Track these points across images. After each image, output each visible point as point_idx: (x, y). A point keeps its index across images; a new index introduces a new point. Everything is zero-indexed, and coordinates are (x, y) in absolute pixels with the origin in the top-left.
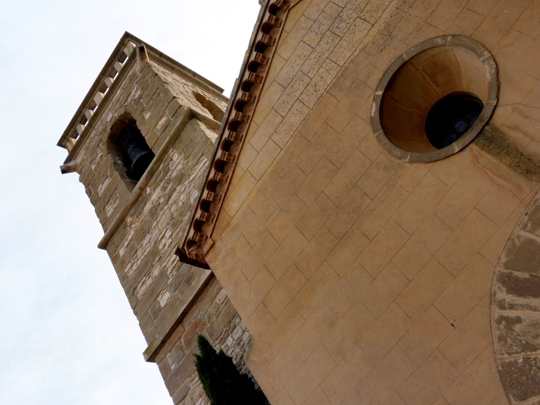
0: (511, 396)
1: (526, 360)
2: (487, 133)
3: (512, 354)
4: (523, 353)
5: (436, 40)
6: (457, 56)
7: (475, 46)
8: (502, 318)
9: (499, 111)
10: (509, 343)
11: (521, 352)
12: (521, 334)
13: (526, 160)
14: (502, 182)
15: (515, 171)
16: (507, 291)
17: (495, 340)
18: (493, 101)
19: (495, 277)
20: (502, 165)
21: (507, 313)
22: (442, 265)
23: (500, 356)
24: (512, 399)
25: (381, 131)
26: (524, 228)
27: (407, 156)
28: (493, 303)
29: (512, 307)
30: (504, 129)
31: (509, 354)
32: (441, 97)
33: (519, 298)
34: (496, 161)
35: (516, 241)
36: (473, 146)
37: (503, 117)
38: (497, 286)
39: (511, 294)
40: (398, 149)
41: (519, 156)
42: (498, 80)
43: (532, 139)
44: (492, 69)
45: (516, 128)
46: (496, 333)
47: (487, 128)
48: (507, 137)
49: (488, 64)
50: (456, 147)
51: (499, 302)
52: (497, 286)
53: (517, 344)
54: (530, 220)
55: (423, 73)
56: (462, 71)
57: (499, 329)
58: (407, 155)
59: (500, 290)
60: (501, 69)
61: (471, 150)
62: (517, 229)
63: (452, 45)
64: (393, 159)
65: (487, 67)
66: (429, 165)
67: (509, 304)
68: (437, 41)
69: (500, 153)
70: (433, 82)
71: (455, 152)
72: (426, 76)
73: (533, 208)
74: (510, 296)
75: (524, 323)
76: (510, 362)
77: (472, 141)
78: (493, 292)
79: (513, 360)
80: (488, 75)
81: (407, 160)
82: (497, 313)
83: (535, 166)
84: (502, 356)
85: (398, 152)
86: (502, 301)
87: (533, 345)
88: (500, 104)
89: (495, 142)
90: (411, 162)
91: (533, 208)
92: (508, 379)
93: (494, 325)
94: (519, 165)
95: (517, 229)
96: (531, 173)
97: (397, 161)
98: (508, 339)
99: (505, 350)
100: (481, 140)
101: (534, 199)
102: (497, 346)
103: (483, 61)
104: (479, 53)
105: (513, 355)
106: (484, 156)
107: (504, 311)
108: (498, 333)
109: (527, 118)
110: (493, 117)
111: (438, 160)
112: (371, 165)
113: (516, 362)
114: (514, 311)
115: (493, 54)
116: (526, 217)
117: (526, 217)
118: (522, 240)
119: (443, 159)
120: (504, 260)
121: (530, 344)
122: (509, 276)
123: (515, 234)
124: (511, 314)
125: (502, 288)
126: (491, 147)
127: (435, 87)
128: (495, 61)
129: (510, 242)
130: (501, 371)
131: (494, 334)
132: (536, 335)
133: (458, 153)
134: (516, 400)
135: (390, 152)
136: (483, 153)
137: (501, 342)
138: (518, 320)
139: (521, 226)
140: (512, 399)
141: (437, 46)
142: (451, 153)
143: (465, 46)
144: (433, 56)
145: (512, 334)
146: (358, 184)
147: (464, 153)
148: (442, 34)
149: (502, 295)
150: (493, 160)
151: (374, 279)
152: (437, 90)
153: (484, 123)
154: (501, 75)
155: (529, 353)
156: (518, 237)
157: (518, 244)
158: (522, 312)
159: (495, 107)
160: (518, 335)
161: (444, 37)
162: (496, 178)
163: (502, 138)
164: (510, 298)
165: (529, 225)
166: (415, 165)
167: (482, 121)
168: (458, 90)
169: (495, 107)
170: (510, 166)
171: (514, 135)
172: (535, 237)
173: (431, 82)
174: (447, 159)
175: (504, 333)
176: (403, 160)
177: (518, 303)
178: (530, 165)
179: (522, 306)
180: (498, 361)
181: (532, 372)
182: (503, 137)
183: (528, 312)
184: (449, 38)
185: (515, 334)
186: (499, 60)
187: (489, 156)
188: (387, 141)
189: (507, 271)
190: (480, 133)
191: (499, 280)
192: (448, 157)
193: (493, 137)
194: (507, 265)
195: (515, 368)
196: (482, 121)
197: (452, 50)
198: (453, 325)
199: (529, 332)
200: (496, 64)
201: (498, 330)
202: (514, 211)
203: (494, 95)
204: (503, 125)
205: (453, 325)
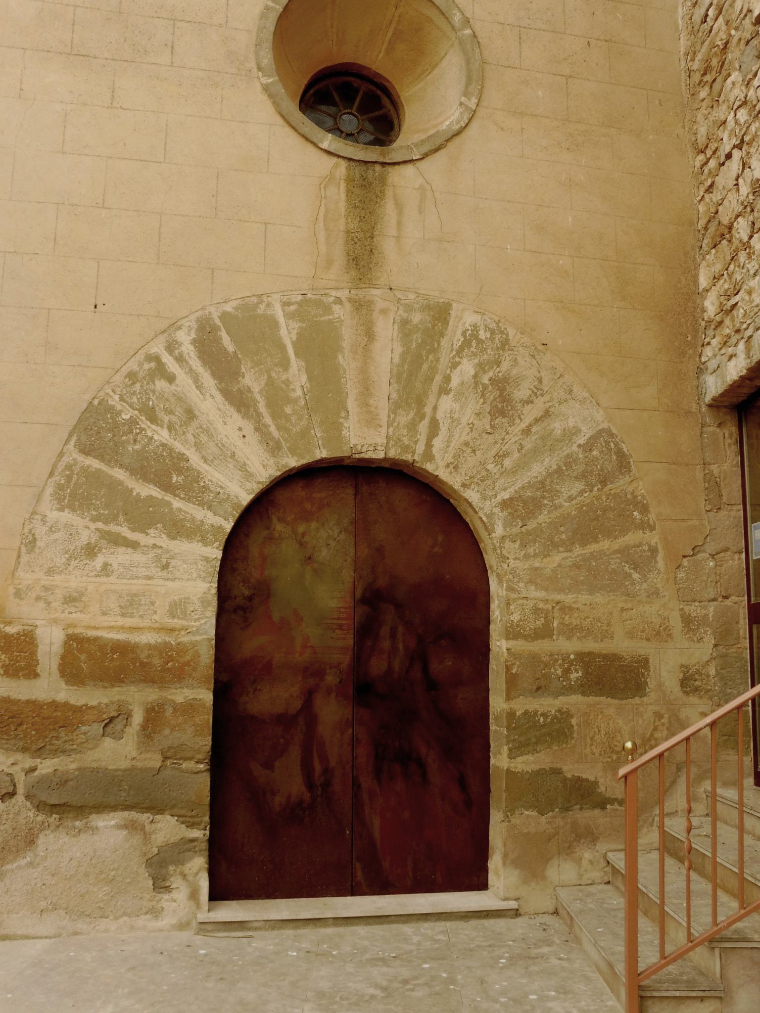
0: (74, 438)
1: (133, 421)
2: (370, 172)
3: (125, 401)
4: (136, 412)
5: (456, 11)
6: (448, 57)
7: (475, 79)
8: (157, 359)
9: (409, 169)
10: (134, 389)
11: (137, 409)
12: (157, 393)
13: (368, 248)
14: (322, 236)
15: (347, 243)
16: (194, 339)
17: (125, 370)
18: (416, 153)
19: (199, 314)
20: (342, 221)
21: (167, 359)
22: (160, 233)
23: (109, 391)
24: (72, 442)
25: (280, 9)
26: (286, 304)
27: (269, 76)
28: (166, 334)
29: (180, 359)
30: (389, 193)
31: (122, 399)
32: (374, 68)
33: (197, 360)
34: (343, 210)
35: (262, 306)
36: (343, 164)
37: (404, 180)
38: (189, 323)
39: (195, 347)
40: (270, 56)
41: (368, 235)
42: (447, 141)
43: (398, 238)
44: (458, 123)
45: (399, 207)
46: (133, 365)
47: (378, 168)
48: (382, 203)
49: (461, 113)
50: (328, 141)
51: (174, 341)
52: (189, 323)
53: (141, 398)
54: (300, 304)
55: (396, 18)
56: (429, 78)
57: (141, 364)
58: (272, 76)
59: (189, 331)
60: (463, 135)
61: (336, 166)
62: (276, 296)
63: (461, 42)
64: (252, 57)
65: (457, 114)
66: (280, 121)
67: (181, 355)
68: (455, 15)
69: (356, 207)
70: (390, 42)
71: (320, 145)
72: (394, 25)
73: (316, 297)
74: (192, 348)
75: (173, 387)
76: (113, 406)
77: (350, 159)
78: (179, 324)
79: (119, 408)
80: (447, 123)
81: (265, 80)
82: (158, 347)
83: (368, 264)
84: (112, 394)
85: (267, 59)
86: (177, 343)
87: (156, 416)
88: (418, 164)
89: (366, 193)
90: (266, 88)
91: (316, 297)
92: (92, 420)
93: (141, 355)
94: (356, 243)
95: (276, 296)
96: (356, 265)
97: (252, 65)
98: (138, 385)
99: (122, 391)
100: (358, 170)
101: (327, 291)
102: (118, 378)
103: (461, 104)
104: (470, 89)
105: (125, 404)
106: (339, 189)
107: (166, 353)
108: (136, 368)
109: (420, 212)
110: (397, 167)
111: (293, 128)
112: (221, 25)
113: (119, 413)
114: (177, 366)
115: (478, 114)
116: (300, 297)
117: (300, 297)
118: (269, 312)
119: (300, 134)
120: (229, 308)
121: (155, 411)
122: (214, 329)
123: (269, 299)
124: (170, 366)
125: (193, 331)
126: (358, 191)
127: (383, 50)
128: (470, 120)
129: (255, 300)
130: (93, 406)
131: (130, 363)
132: (171, 410)
133: (322, 149)
134: (75, 446)
135: (258, 45)
136: (343, 185)
137: (127, 380)
138: (171, 379)
139: (285, 299)
140: (72, 442)
141: (447, 19)
142: (315, 140)
143: (468, 63)
144: (429, 20)
145: (148, 383)
146: (178, 24)
147: (325, 157)
148: (468, 15)
149: (185, 339)
150: (342, 205)
151: (64, 153)
152: (381, 56)
153: (381, 160)
154: (457, 141)
155: (143, 418)
156: (269, 305)
157: (260, 312)
158: (184, 375)
159: (411, 161)
160: (154, 391)
161: (467, 22)
162: (322, 224)
163: (377, 197)
164: (188, 349)
165: (292, 308)
166: (265, 97)
167: (383, 154)
168: (397, 87)
169: (411, 161)
170: (348, 232)
171: (389, 208)
172: (284, 325)
173: (388, 38)
174: (303, 140)
175: (141, 375)
176: (260, 74)
177: (191, 362)
178: (365, 257)
179: (191, 369)
180: (102, 394)
181: (124, 438)
182: (380, 196)
183: (190, 381)
184: (468, 31)
185: (152, 387)
186: (474, 125)
187: (343, 196)
188: (272, 29)
189: (218, 322)
190: (366, 162)
191: (198, 320)
192: (307, 139)
193: (370, 184)
194: (224, 316)
195: (112, 418)
196: (383, 154)
197: (452, 46)
198: (96, 307)
199: (168, 400)
200: (467, 125)
201: (139, 365)
202: (296, 277)
203: (425, 149)
204: (394, 186)
205: (96, 307)
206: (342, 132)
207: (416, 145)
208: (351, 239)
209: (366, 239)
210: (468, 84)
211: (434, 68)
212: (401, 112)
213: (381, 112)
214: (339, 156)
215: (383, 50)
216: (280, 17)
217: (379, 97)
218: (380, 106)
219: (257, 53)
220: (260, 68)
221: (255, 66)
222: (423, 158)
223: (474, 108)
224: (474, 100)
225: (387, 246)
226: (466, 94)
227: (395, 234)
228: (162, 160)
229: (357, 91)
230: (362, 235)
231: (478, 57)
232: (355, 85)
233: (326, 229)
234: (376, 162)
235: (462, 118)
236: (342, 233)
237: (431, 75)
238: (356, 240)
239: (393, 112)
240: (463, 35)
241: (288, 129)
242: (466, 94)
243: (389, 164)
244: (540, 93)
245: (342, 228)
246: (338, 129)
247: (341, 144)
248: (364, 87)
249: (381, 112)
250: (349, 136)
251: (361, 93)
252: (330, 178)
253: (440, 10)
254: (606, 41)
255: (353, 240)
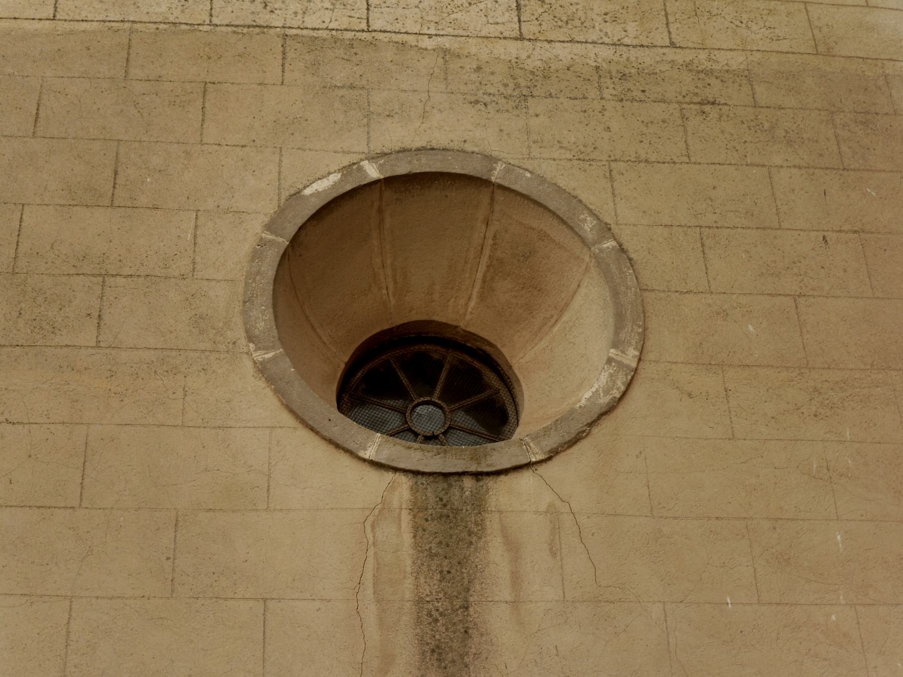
2: (456, 491)
5: (585, 215)
6: (583, 291)
7: (632, 318)
9: (525, 481)
14: (371, 612)
15: (418, 621)
20: (409, 582)
22: (68, 632)
27: (267, 349)
30: (492, 523)
32: (462, 325)
34: (409, 562)
36: (405, 482)
37: (519, 501)
41: (457, 603)
42: (591, 424)
43: (515, 603)
45: (514, 548)
47: (468, 482)
49: (611, 375)
50: (375, 445)
56: (556, 329)
60: (619, 412)
61: (392, 487)
63: (599, 260)
64: (238, 320)
65: (604, 378)
66: (287, 419)
70: (484, 281)
71: (362, 454)
72: (487, 252)
77: (416, 473)
80: (588, 395)
83: (462, 656)
89: (449, 528)
90: (262, 369)
94: (437, 620)
96: (439, 660)
97: (239, 333)
100: (431, 491)
103: (610, 361)
104: (622, 336)
106: (400, 528)
109: (553, 554)
110: (503, 478)
111: (312, 429)
112: (183, 277)
115: (641, 371)
119: (324, 438)
126: (432, 526)
127: (475, 293)
133: (364, 460)
135: (247, 301)
136: (406, 518)
141: (571, 228)
142: (352, 446)
143: (615, 294)
144: (543, 236)
147: (373, 475)
152: (472, 304)
153: (473, 468)
154: (607, 424)
159: (529, 465)
161: (606, 230)
162: (370, 591)
163: (470, 533)
166: (262, 384)
168: (504, 351)
169: (529, 465)
170: (419, 601)
171: (494, 554)
174: (331, 449)
176: (251, 345)
178: (455, 645)
182: (474, 535)
184: (610, 244)
186: (637, 392)
187: (407, 538)
188: (271, 274)
190: (446, 475)
192: (337, 446)
196: (475, 458)
200: (624, 394)
203: (553, 441)
204: (500, 512)
206: (416, 435)
207: (535, 437)
208: (428, 615)
209: (455, 611)
210: (619, 326)
211: (562, 311)
212: (516, 391)
213: (481, 396)
214: (396, 470)
215: (475, 293)
216: (285, 256)
217: (478, 374)
218: (479, 384)
219: (245, 313)
220: (250, 338)
221: (243, 335)
222: (549, 459)
223: (634, 365)
224: (633, 352)
225: (496, 619)
226: (616, 344)
227: (509, 598)
228: (76, 503)
229: (440, 365)
230: (447, 604)
231: (631, 281)
232: (436, 356)
233: (379, 601)
234: (464, 474)
235: (614, 383)
236: (408, 605)
237: (559, 325)
238: (435, 614)
239: (504, 394)
240: (601, 251)
241: (303, 434)
242: (616, 344)
243: (488, 474)
244: (751, 328)
245: (408, 595)
246: (410, 430)
247: (398, 448)
248: (451, 357)
249: (481, 396)
250: (429, 439)
251: (447, 367)
252: (383, 509)
253: (558, 217)
254: (855, 232)
255: (430, 614)
